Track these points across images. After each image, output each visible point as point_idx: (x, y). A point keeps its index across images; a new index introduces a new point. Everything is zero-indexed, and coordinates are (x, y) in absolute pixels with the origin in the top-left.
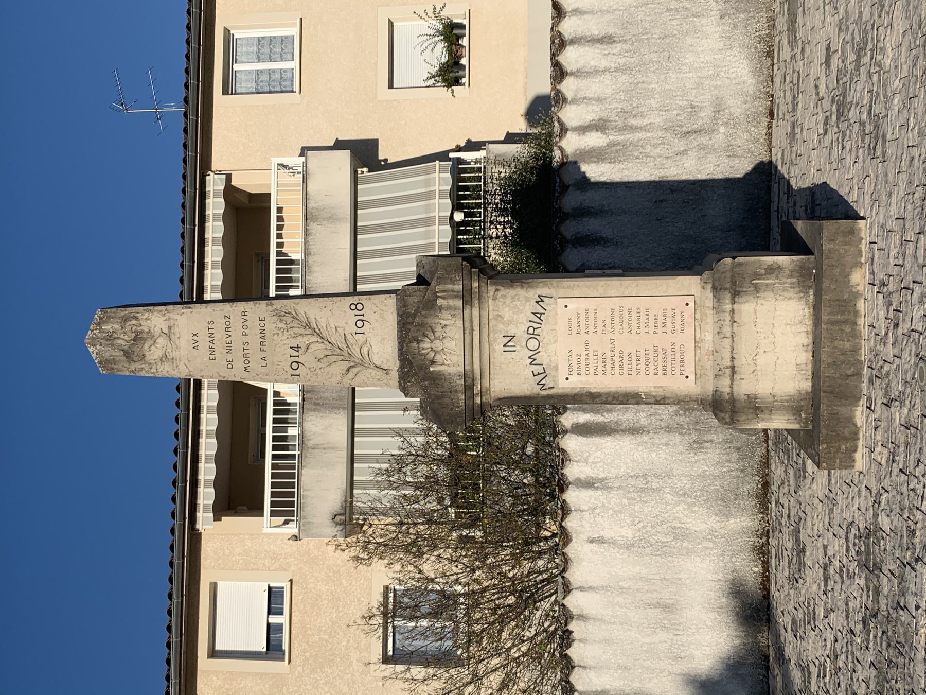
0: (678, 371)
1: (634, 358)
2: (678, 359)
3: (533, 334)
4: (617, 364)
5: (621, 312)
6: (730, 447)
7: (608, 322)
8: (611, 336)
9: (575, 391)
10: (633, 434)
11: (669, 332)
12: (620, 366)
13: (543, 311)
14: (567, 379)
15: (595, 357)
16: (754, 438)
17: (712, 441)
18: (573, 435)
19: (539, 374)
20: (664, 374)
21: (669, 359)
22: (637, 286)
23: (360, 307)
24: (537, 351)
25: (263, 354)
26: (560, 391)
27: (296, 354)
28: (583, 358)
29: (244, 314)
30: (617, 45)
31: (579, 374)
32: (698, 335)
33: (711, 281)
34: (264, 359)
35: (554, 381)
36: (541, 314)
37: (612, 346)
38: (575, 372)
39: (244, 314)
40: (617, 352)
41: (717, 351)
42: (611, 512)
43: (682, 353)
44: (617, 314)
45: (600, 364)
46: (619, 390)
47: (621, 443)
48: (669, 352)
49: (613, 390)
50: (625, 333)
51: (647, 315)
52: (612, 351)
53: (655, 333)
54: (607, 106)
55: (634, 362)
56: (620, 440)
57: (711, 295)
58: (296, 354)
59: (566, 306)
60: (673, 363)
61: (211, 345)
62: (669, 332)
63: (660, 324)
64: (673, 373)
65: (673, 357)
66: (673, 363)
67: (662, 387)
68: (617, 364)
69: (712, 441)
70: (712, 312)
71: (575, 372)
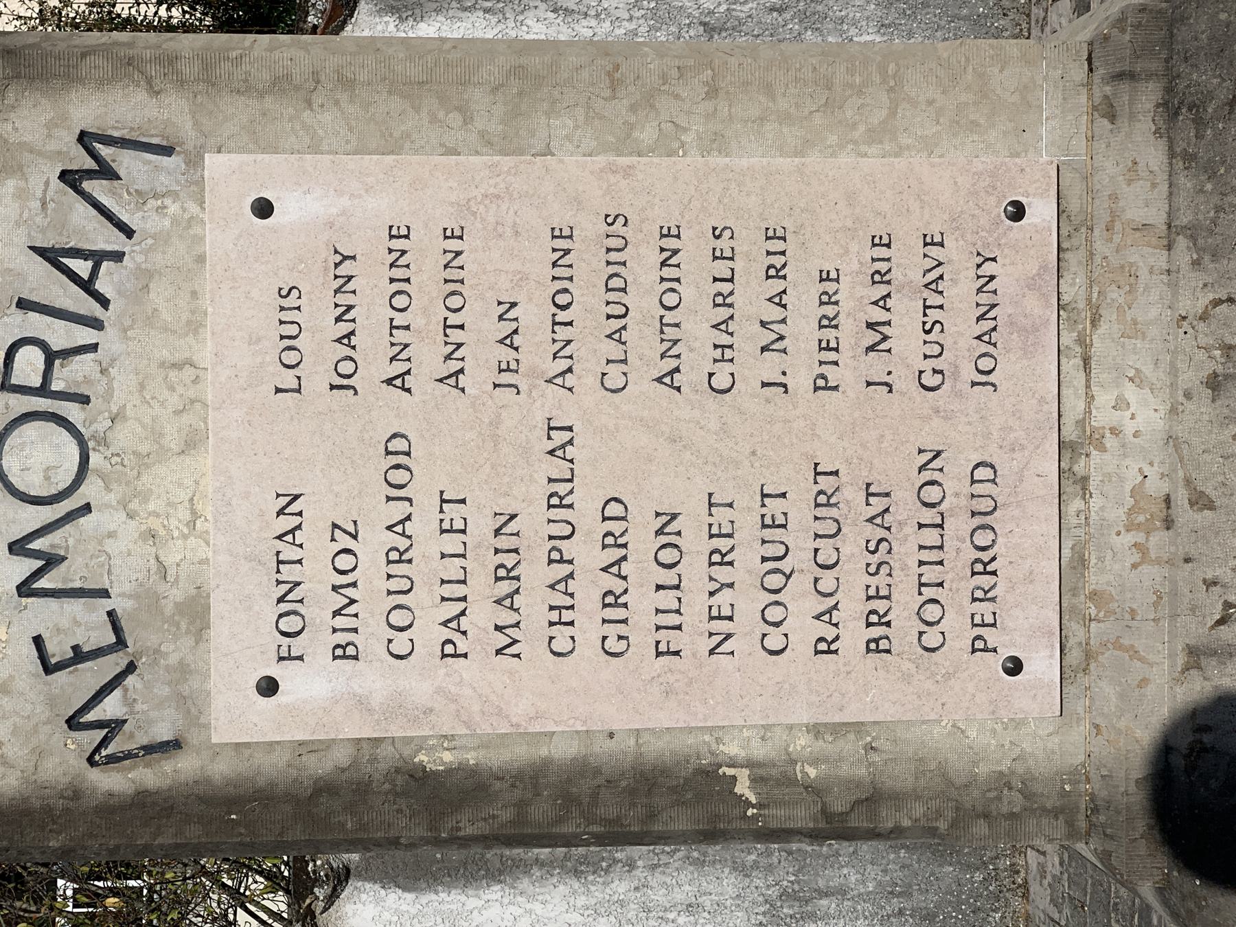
1: (696, 544)
2: (960, 554)
3: (43, 390)
4: (588, 591)
5: (615, 251)
6: (901, 912)
8: (550, 402)
9: (320, 766)
10: (577, 874)
11: (904, 382)
12: (611, 600)
13: (108, 239)
14: (269, 687)
15: (452, 544)
16: (979, 877)
17: (842, 892)
18: (368, 886)
19: (79, 656)
20: (874, 647)
21: (906, 550)
22: (712, 92)
26: (221, 769)
31: (342, 653)
32: (1075, 406)
33: (1155, 65)
35: (182, 700)
36: (97, 257)
37: (558, 468)
38: (317, 644)
41: (1201, 502)
43: (983, 519)
45: (481, 587)
46: (602, 747)
47: (537, 907)
48: (905, 509)
49: (563, 751)
50: (642, 384)
51: (775, 273)
52: (557, 502)
53: (822, 385)
55: (694, 570)
56: (531, 898)
57: (1154, 156)
59: (263, 209)
60: (930, 574)
62: (904, 382)
63: (850, 334)
64: (932, 639)
65: (931, 536)
66: (930, 574)
67: (858, 728)
68: (588, 591)
69: (842, 892)
70: (1160, 259)
71: (317, 644)
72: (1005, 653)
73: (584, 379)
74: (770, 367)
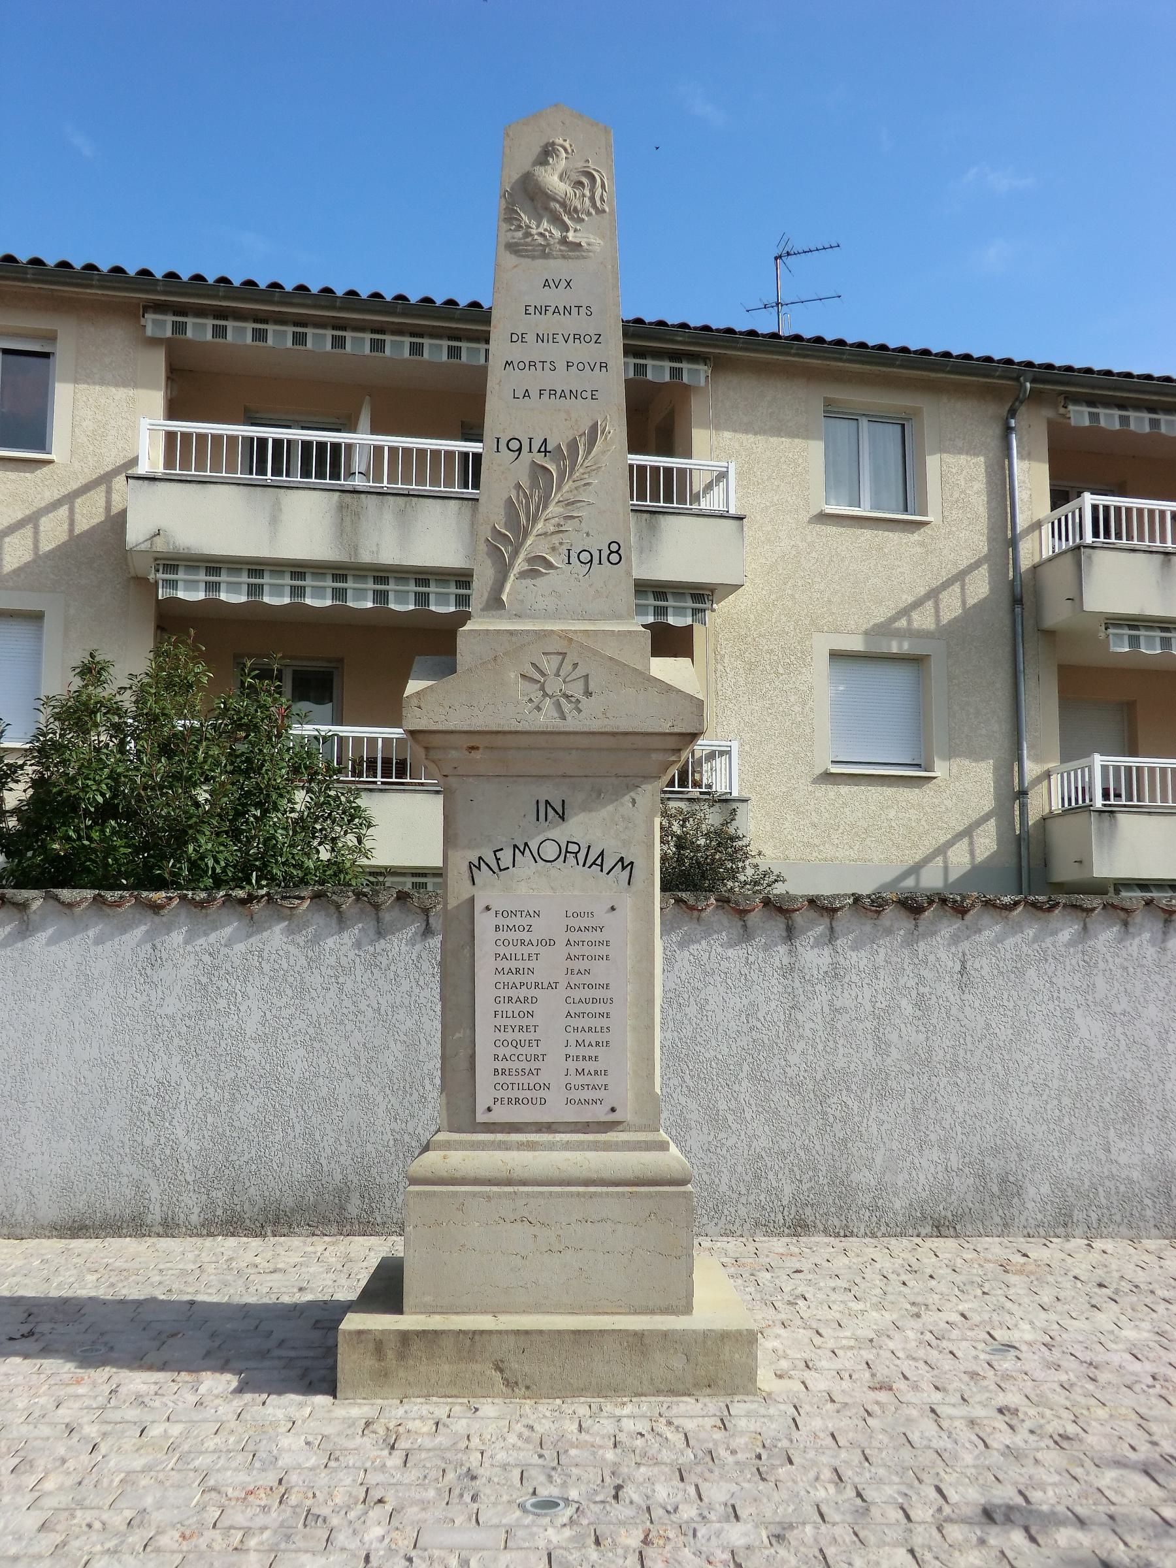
0: (500, 1094)
1: (525, 1022)
2: (521, 1095)
3: (567, 852)
4: (513, 993)
7: (586, 979)
12: (510, 999)
15: (526, 957)
19: (498, 860)
20: (496, 1070)
23: (614, 558)
24: (537, 857)
25: (534, 394)
27: (535, 448)
28: (526, 936)
29: (604, 366)
30: (957, 997)
34: (527, 394)
36: (602, 866)
38: (500, 921)
39: (604, 366)
40: (534, 992)
42: (204, 980)
43: (530, 1101)
44: (599, 993)
45: (513, 964)
48: (533, 1080)
53: (567, 1057)
54: (867, 981)
55: (518, 1022)
58: (535, 448)
61: (551, 310)
63: (581, 1065)
65: (526, 1087)
68: (513, 993)
71: (500, 921)
72: (493, 1107)
73: (569, 992)
74: (572, 1043)
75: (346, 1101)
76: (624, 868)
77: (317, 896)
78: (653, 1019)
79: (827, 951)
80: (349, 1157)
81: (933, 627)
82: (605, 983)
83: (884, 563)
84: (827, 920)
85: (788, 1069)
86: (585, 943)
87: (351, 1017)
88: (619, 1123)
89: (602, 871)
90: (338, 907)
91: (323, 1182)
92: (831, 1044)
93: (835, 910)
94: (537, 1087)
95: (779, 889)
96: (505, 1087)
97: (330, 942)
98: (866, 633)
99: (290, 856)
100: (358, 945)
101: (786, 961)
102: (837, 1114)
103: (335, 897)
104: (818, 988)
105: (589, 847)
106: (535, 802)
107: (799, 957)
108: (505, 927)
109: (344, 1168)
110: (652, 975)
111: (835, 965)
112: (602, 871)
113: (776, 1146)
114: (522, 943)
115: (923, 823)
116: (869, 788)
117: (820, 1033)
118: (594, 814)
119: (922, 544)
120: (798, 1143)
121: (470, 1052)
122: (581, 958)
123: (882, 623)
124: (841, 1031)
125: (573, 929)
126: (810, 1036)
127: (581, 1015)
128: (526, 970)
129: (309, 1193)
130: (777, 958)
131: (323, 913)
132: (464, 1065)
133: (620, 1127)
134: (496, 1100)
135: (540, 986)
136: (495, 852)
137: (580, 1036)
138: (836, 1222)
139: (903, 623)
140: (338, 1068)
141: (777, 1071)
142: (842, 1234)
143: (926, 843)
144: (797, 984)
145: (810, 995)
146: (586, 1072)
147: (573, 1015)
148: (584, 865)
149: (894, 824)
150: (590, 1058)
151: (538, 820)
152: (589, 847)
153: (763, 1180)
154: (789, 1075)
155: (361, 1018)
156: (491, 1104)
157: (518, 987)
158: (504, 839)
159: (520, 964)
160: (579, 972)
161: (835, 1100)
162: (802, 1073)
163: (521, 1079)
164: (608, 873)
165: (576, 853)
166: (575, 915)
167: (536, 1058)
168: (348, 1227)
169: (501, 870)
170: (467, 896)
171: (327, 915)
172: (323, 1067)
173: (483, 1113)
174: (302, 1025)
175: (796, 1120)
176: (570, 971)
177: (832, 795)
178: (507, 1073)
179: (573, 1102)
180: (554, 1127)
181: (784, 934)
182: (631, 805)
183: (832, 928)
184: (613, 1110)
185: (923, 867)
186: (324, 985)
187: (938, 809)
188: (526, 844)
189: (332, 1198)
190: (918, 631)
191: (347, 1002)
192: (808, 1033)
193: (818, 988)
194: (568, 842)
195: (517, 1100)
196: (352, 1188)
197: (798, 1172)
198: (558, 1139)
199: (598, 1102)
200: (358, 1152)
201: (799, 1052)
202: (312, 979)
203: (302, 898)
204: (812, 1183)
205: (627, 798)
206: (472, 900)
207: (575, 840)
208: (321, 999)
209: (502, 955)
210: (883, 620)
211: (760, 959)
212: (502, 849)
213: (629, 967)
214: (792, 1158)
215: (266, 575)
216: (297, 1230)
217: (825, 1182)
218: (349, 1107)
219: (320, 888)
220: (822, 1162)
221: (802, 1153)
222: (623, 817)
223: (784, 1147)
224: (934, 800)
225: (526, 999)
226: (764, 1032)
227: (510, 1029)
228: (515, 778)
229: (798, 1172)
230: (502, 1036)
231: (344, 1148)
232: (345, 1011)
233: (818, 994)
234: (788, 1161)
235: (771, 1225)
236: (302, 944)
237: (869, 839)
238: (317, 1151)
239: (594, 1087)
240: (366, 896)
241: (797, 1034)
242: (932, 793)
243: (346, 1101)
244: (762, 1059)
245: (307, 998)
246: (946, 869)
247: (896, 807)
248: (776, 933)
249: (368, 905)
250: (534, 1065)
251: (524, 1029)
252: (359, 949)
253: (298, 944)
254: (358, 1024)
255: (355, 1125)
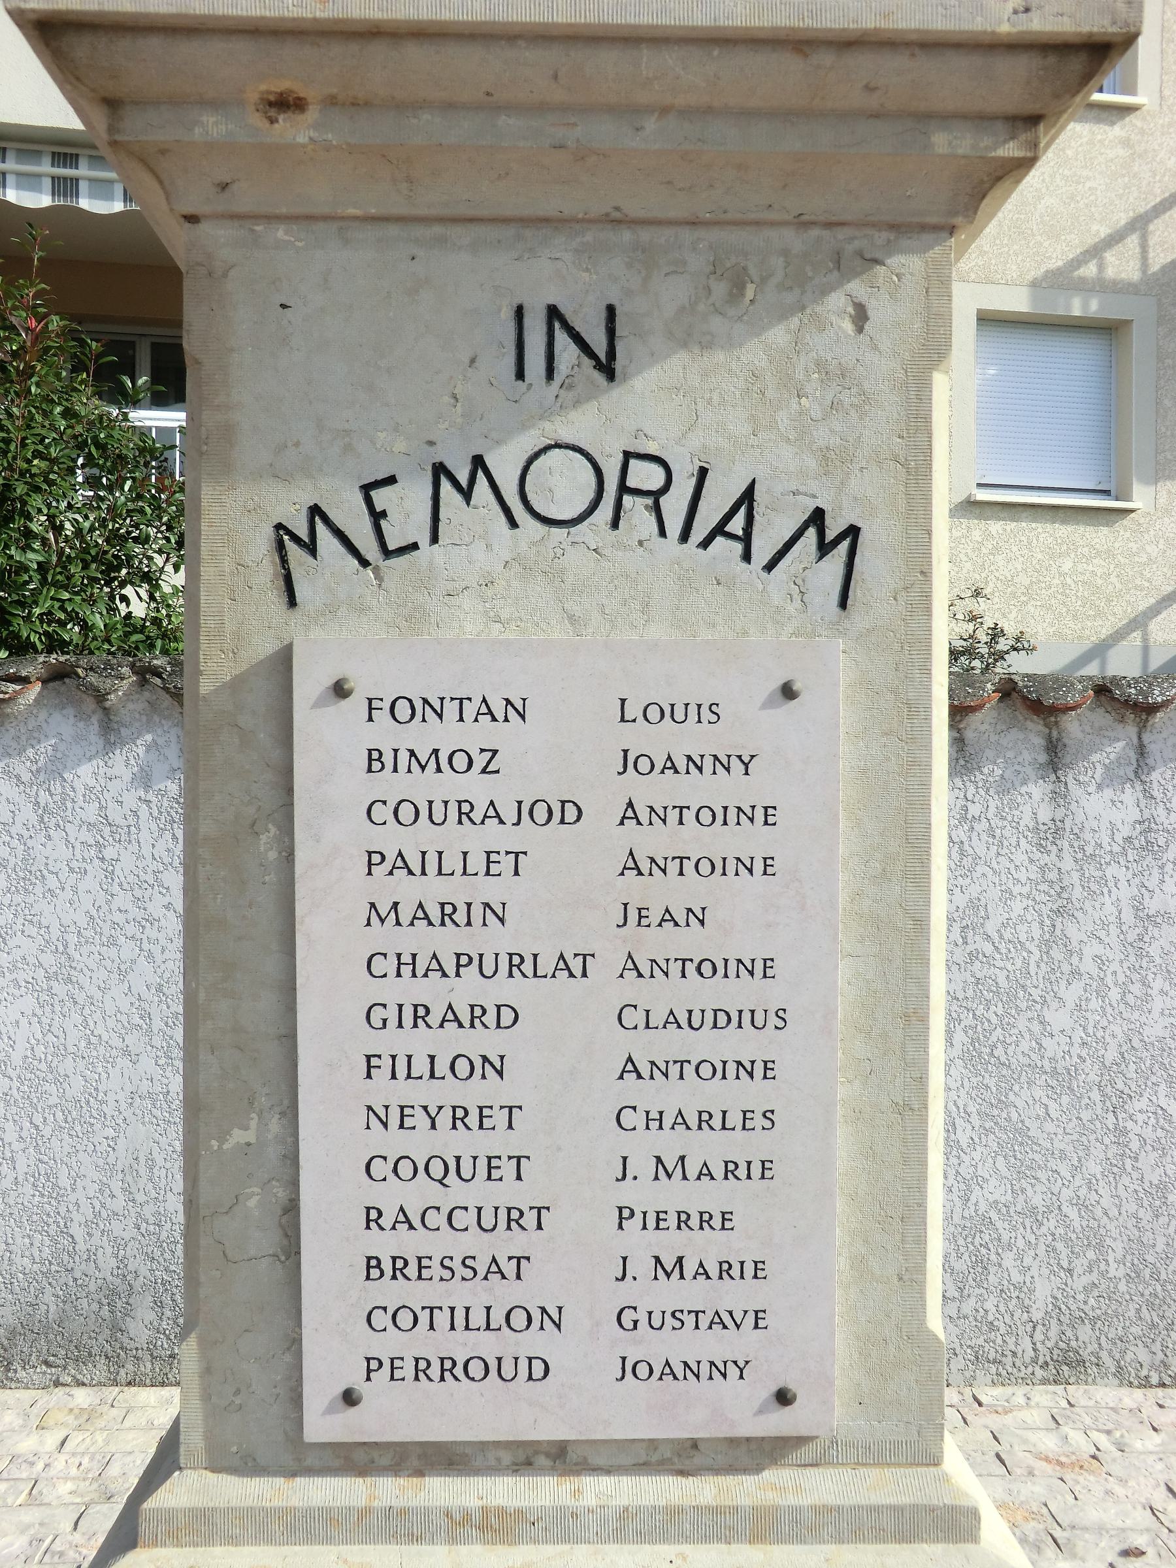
0: (388, 1344)
1: (473, 1094)
2: (460, 1346)
12: (421, 1014)
15: (477, 863)
19: (378, 516)
20: (372, 1263)
36: (746, 539)
40: (504, 990)
48: (503, 1295)
53: (623, 1215)
55: (448, 1092)
63: (670, 1243)
65: (478, 1319)
73: (631, 989)
74: (642, 1165)
75: (123, 1106)
76: (824, 548)
77: (57, 676)
78: (922, 1081)
79: (1130, 795)
80: (131, 1222)
81: (1136, 276)
82: (759, 956)
83: (1066, 172)
84: (1132, 730)
85: (1046, 1042)
86: (689, 816)
87: (131, 929)
88: (801, 1441)
89: (747, 557)
90: (100, 697)
91: (78, 1274)
92: (1136, 989)
93: (1152, 709)
94: (519, 1320)
95: (1019, 665)
96: (405, 1319)
97: (86, 773)
98: (1034, 284)
99: (57, 605)
100: (144, 779)
101: (1045, 815)
102: (1148, 1133)
103: (93, 678)
104: (1110, 871)
105: (703, 472)
106: (507, 314)
107: (1074, 806)
108: (403, 757)
109: (118, 1244)
110: (921, 924)
111: (1146, 825)
112: (747, 557)
113: (1021, 1198)
114: (465, 815)
115: (1113, 579)
116: (1034, 525)
117: (1115, 966)
118: (720, 356)
119: (1126, 143)
120: (1066, 1193)
121: (281, 1193)
122: (673, 867)
123: (1058, 269)
124: (1158, 961)
125: (644, 765)
126: (1095, 971)
127: (674, 1070)
128: (477, 911)
129: (48, 1297)
130: (1027, 810)
131: (70, 711)
132: (266, 1241)
133: (806, 1453)
134: (372, 1366)
135: (528, 967)
136: (367, 489)
137: (670, 1143)
138: (1143, 1355)
139: (1090, 270)
140: (105, 1037)
141: (1025, 1046)
142: (1154, 1380)
143: (1118, 610)
144: (1068, 864)
145: (1094, 887)
146: (690, 1267)
147: (645, 1071)
148: (685, 536)
149: (1069, 581)
150: (705, 1220)
151: (520, 375)
152: (703, 472)
153: (992, 1270)
154: (1049, 1054)
155: (151, 932)
156: (355, 1377)
157: (450, 969)
158: (400, 446)
159: (455, 890)
160: (668, 917)
161: (1143, 1104)
162: (1076, 1050)
163: (460, 1294)
164: (770, 567)
165: (657, 495)
166: (653, 713)
167: (514, 1219)
168: (130, 1367)
169: (387, 553)
170: (264, 647)
171: (81, 716)
172: (74, 1036)
173: (330, 1410)
174: (28, 947)
175: (1062, 1146)
176: (633, 916)
177: (977, 535)
178: (412, 1271)
179: (643, 1370)
180: (572, 1456)
181: (1043, 758)
182: (848, 326)
183: (1141, 750)
184: (783, 1398)
185: (1111, 646)
186: (74, 864)
187: (1137, 559)
188: (478, 462)
189: (95, 1306)
190: (1115, 283)
191: (123, 900)
192: (1088, 966)
193: (1110, 871)
194: (627, 455)
195: (448, 1367)
196: (137, 1285)
197: (1065, 1253)
198: (589, 1500)
199: (733, 1372)
200: (148, 1211)
201: (1070, 1005)
202: (48, 851)
203: (25, 680)
204: (1094, 1277)
205: (837, 301)
206: (284, 659)
207: (652, 449)
208: (68, 894)
209: (391, 856)
210: (1060, 263)
211: (992, 810)
212: (391, 480)
213: (842, 899)
214: (1053, 1222)
215: (83, 162)
216: (21, 1374)
217: (1121, 1273)
218: (131, 1119)
219: (62, 659)
220: (1115, 1233)
221: (1073, 1213)
222: (820, 365)
223: (1037, 1201)
224: (1131, 545)
225: (477, 1014)
226: (999, 964)
227: (421, 1120)
228: (437, 229)
229: (1065, 1253)
230: (394, 1142)
231: (119, 1204)
232: (119, 918)
233: (1111, 884)
234: (1044, 1230)
235: (1008, 1360)
236: (26, 777)
237: (1033, 602)
238: (63, 1210)
239: (717, 1321)
240: (159, 676)
241: (1066, 968)
242: (1128, 534)
243: (123, 1106)
244: (994, 1020)
245: (39, 890)
246: (1146, 649)
247: (1072, 556)
248: (1027, 756)
249: (163, 693)
250: (506, 1244)
251: (472, 1120)
252: (147, 787)
253: (18, 777)
254: (146, 946)
255: (142, 1160)
